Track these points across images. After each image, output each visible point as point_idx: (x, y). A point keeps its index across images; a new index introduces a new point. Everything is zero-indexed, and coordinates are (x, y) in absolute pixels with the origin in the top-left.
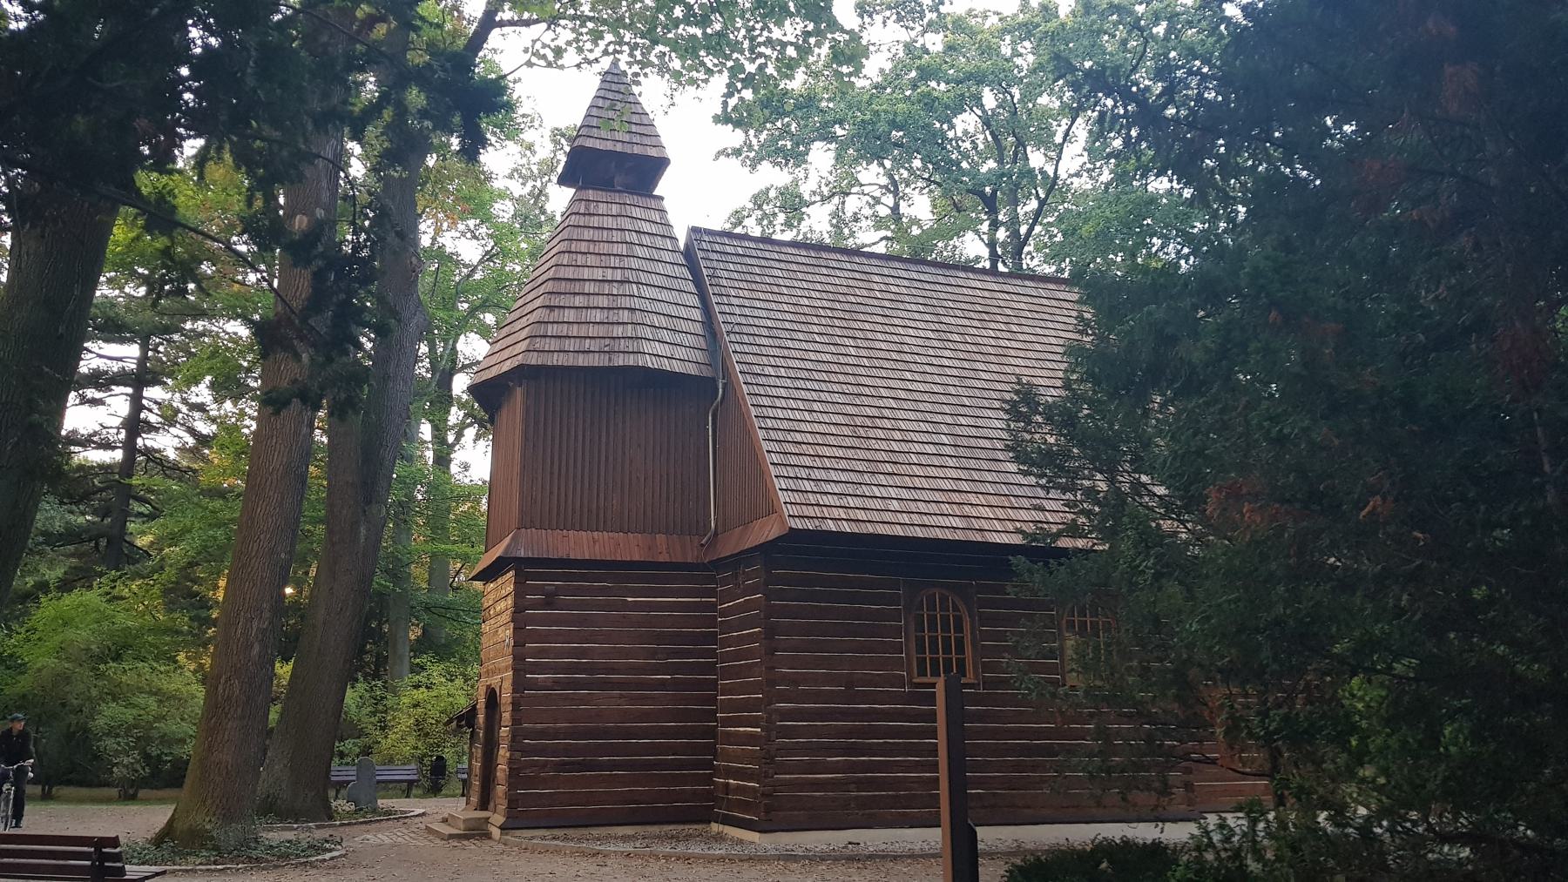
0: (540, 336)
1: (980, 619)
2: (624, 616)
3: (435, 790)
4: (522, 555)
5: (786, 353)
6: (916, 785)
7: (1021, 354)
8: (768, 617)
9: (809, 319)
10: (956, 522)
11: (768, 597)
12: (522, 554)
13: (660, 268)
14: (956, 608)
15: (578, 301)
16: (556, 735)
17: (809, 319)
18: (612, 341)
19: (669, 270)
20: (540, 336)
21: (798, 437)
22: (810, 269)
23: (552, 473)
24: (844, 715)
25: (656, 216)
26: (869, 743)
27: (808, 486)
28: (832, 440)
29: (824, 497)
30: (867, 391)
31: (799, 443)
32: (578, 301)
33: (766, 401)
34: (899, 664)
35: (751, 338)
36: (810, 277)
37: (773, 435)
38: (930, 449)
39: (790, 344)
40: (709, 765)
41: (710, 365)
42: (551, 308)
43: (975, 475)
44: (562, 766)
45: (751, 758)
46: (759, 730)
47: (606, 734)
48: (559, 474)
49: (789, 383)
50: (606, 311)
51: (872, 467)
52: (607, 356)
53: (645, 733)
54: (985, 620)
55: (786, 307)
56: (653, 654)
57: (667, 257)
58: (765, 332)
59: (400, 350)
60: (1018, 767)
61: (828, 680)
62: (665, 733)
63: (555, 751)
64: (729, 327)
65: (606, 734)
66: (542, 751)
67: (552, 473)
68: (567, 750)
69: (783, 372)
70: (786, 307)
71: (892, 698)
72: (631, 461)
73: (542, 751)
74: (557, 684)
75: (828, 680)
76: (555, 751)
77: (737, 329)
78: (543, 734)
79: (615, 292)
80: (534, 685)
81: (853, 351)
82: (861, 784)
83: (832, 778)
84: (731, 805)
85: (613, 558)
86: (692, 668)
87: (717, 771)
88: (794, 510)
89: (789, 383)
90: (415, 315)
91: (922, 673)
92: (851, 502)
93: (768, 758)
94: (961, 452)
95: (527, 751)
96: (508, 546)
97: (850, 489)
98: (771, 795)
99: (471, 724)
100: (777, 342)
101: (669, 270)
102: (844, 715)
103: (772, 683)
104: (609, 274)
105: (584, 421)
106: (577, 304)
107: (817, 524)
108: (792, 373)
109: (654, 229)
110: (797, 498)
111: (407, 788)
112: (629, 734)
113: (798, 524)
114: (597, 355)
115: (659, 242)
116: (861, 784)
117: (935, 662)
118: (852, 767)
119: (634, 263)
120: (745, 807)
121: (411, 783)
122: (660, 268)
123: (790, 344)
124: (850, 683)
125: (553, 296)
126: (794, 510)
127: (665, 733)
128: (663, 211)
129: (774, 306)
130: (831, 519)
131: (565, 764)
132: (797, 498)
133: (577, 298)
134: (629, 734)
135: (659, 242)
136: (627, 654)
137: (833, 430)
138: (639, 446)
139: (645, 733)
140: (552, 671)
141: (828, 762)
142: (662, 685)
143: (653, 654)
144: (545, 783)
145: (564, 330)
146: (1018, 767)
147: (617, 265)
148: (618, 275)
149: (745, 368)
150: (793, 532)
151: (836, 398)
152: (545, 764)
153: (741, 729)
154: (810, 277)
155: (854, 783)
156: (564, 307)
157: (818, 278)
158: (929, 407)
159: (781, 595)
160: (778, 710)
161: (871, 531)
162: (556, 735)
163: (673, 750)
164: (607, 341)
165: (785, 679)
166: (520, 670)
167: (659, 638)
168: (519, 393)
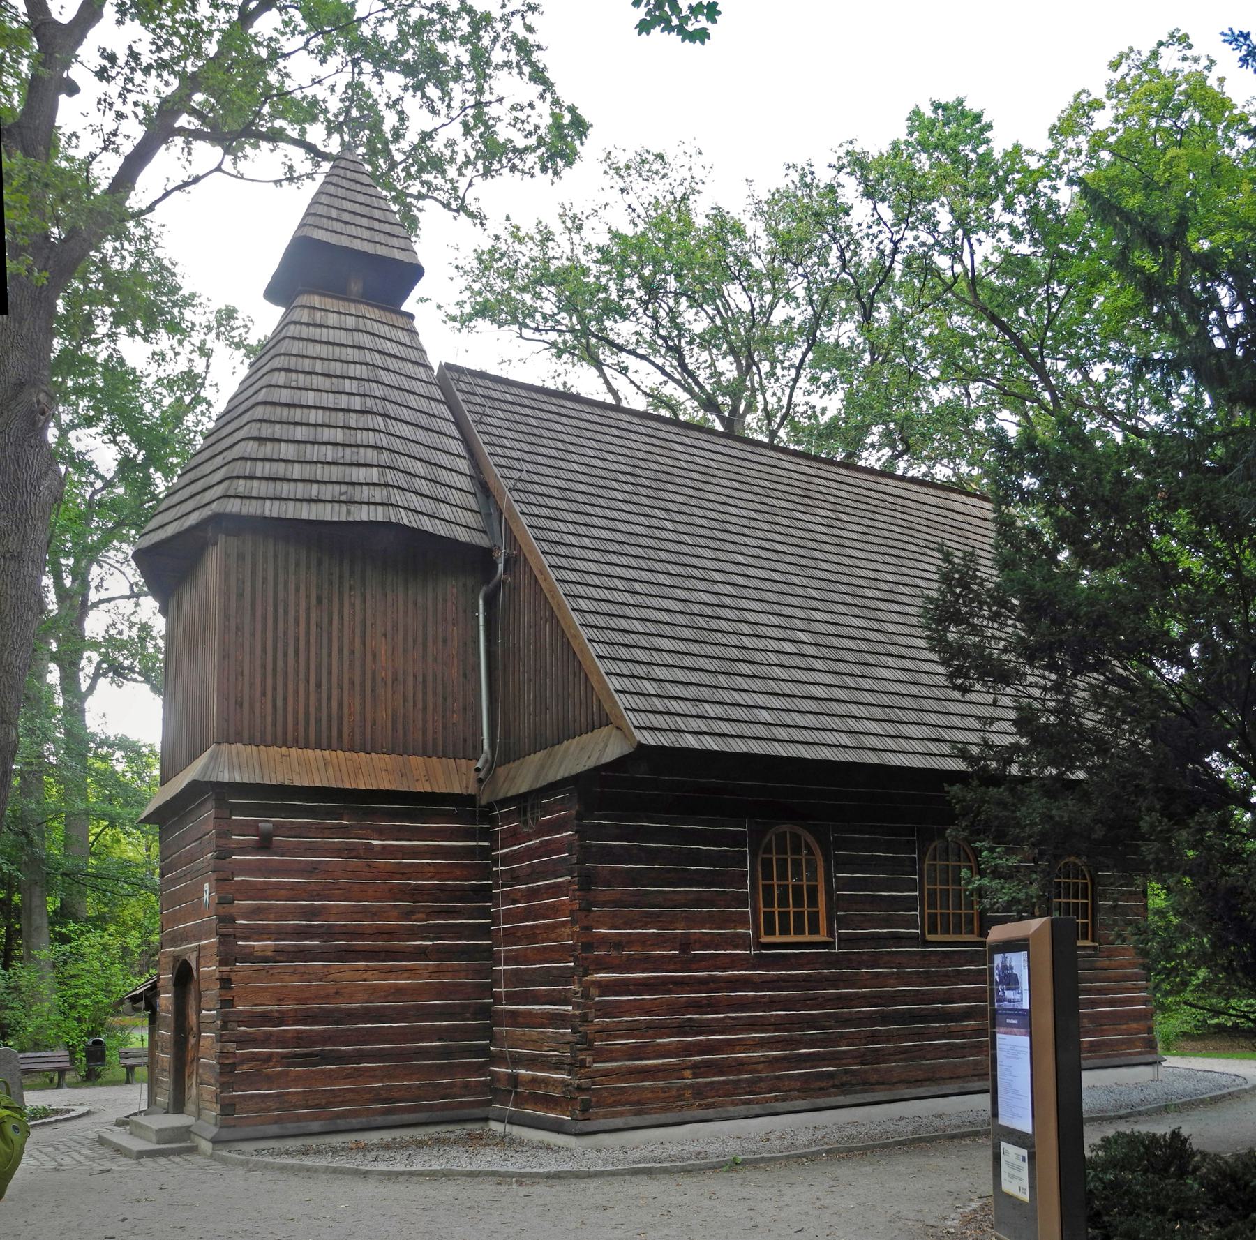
0: (245, 478)
1: (837, 864)
2: (368, 865)
3: (91, 1078)
4: (226, 780)
5: (587, 519)
6: (761, 1066)
7: (859, 545)
8: (582, 861)
9: (608, 484)
10: (844, 739)
11: (582, 833)
12: (226, 777)
13: (413, 401)
14: (811, 852)
15: (300, 433)
16: (282, 1019)
17: (608, 484)
18: (351, 488)
19: (424, 404)
20: (245, 478)
21: (624, 624)
22: (599, 428)
23: (264, 667)
24: (679, 984)
25: (403, 337)
26: (708, 1020)
27: (649, 687)
28: (667, 630)
29: (674, 703)
30: (696, 573)
31: (627, 632)
32: (300, 433)
33: (573, 576)
34: (742, 920)
35: (539, 498)
36: (599, 437)
37: (591, 619)
38: (789, 647)
39: (589, 509)
40: (484, 1051)
41: (485, 532)
42: (261, 440)
43: (850, 681)
44: (293, 1060)
45: (558, 1042)
46: (570, 1008)
47: (350, 1016)
48: (275, 670)
49: (597, 556)
50: (340, 448)
51: (728, 666)
52: (344, 507)
53: (402, 1014)
54: (844, 864)
55: (576, 467)
56: (408, 914)
57: (420, 388)
58: (556, 493)
59: (26, 520)
60: (873, 1038)
61: (659, 941)
62: (425, 1013)
63: (282, 1041)
64: (511, 483)
65: (350, 1016)
66: (265, 1040)
67: (264, 667)
68: (299, 1039)
69: (587, 542)
70: (576, 467)
71: (733, 962)
72: (374, 656)
73: (265, 1040)
74: (281, 954)
75: (659, 941)
76: (282, 1041)
77: (519, 485)
78: (265, 1019)
79: (353, 424)
80: (249, 956)
81: (669, 525)
82: (697, 1069)
83: (663, 1064)
84: (520, 1100)
85: (354, 786)
86: (458, 932)
87: (498, 1059)
88: (642, 719)
89: (597, 556)
90: (46, 474)
91: (770, 931)
92: (710, 710)
93: (586, 1042)
94: (825, 652)
95: (242, 1041)
96: (206, 768)
97: (705, 693)
98: (588, 1089)
99: (151, 1007)
100: (574, 507)
101: (424, 404)
102: (679, 984)
103: (588, 947)
104: (344, 401)
105: (308, 597)
106: (298, 438)
107: (673, 739)
108: (598, 544)
109: (401, 351)
110: (640, 702)
111: (56, 1080)
112: (380, 1015)
113: (648, 739)
114: (329, 506)
115: (410, 369)
116: (697, 1069)
117: (784, 916)
118: (687, 1050)
119: (377, 390)
120: (549, 1102)
121: (62, 1072)
122: (413, 401)
123: (589, 509)
124: (685, 945)
125: (264, 425)
126: (642, 719)
127: (425, 1013)
128: (413, 332)
129: (561, 464)
130: (689, 732)
131: (296, 1056)
132: (640, 702)
133: (299, 428)
134: (380, 1015)
135: (410, 369)
136: (375, 915)
137: (665, 617)
138: (385, 635)
139: (402, 1014)
140: (273, 937)
141: (659, 1045)
142: (421, 954)
143: (408, 914)
144: (271, 1080)
145: (279, 469)
146: (873, 1038)
147: (355, 391)
148: (357, 403)
149: (539, 533)
150: (641, 747)
151: (662, 579)
152: (269, 1058)
153: (536, 1007)
154: (599, 437)
155: (688, 1068)
156: (279, 441)
157: (609, 439)
158: (774, 597)
159: (599, 832)
160: (594, 983)
161: (745, 750)
162: (282, 1019)
163: (441, 1034)
164: (344, 488)
165: (604, 942)
166: (229, 935)
167: (416, 893)
168: (214, 557)
